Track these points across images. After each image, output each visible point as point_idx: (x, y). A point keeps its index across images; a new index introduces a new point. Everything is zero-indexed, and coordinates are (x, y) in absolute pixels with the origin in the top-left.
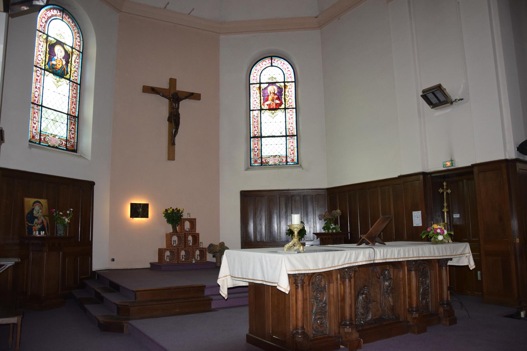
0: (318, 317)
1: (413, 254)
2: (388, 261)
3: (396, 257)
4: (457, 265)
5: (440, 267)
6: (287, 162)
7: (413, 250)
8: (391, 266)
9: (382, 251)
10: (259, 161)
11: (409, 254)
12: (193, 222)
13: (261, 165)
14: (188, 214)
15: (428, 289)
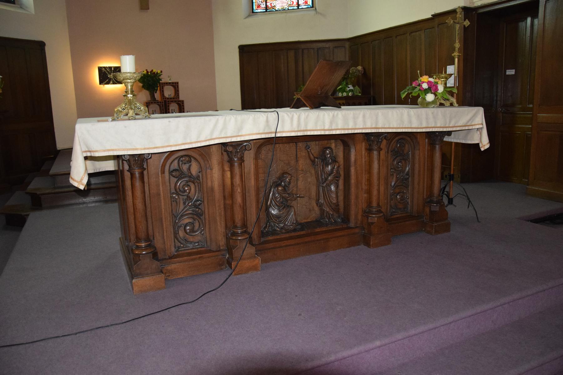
0: (397, 191)
1: (364, 122)
2: (309, 133)
3: (326, 128)
4: (464, 142)
5: (432, 145)
6: (298, 5)
7: (364, 116)
8: (339, 142)
9: (296, 117)
10: (263, 6)
11: (355, 123)
12: (175, 85)
13: (266, 11)
14: (169, 77)
15: (408, 178)
